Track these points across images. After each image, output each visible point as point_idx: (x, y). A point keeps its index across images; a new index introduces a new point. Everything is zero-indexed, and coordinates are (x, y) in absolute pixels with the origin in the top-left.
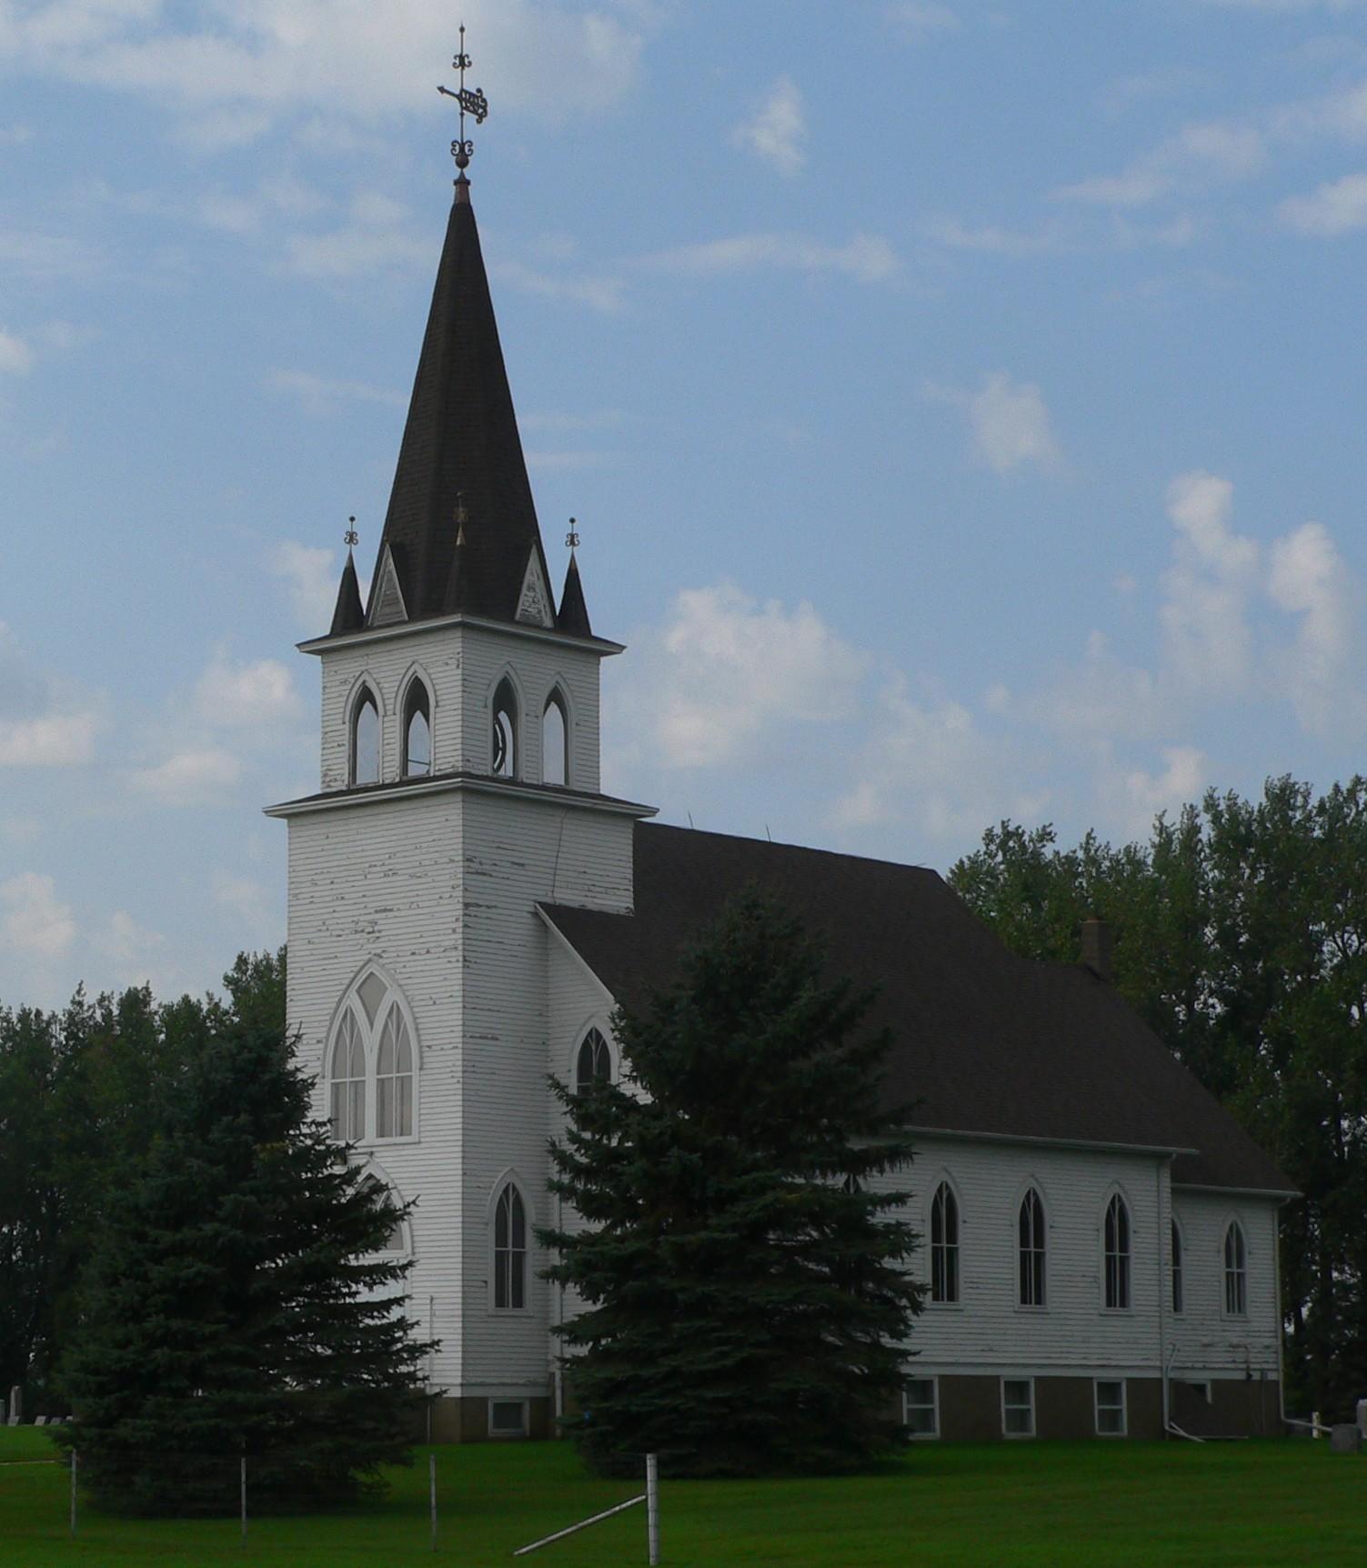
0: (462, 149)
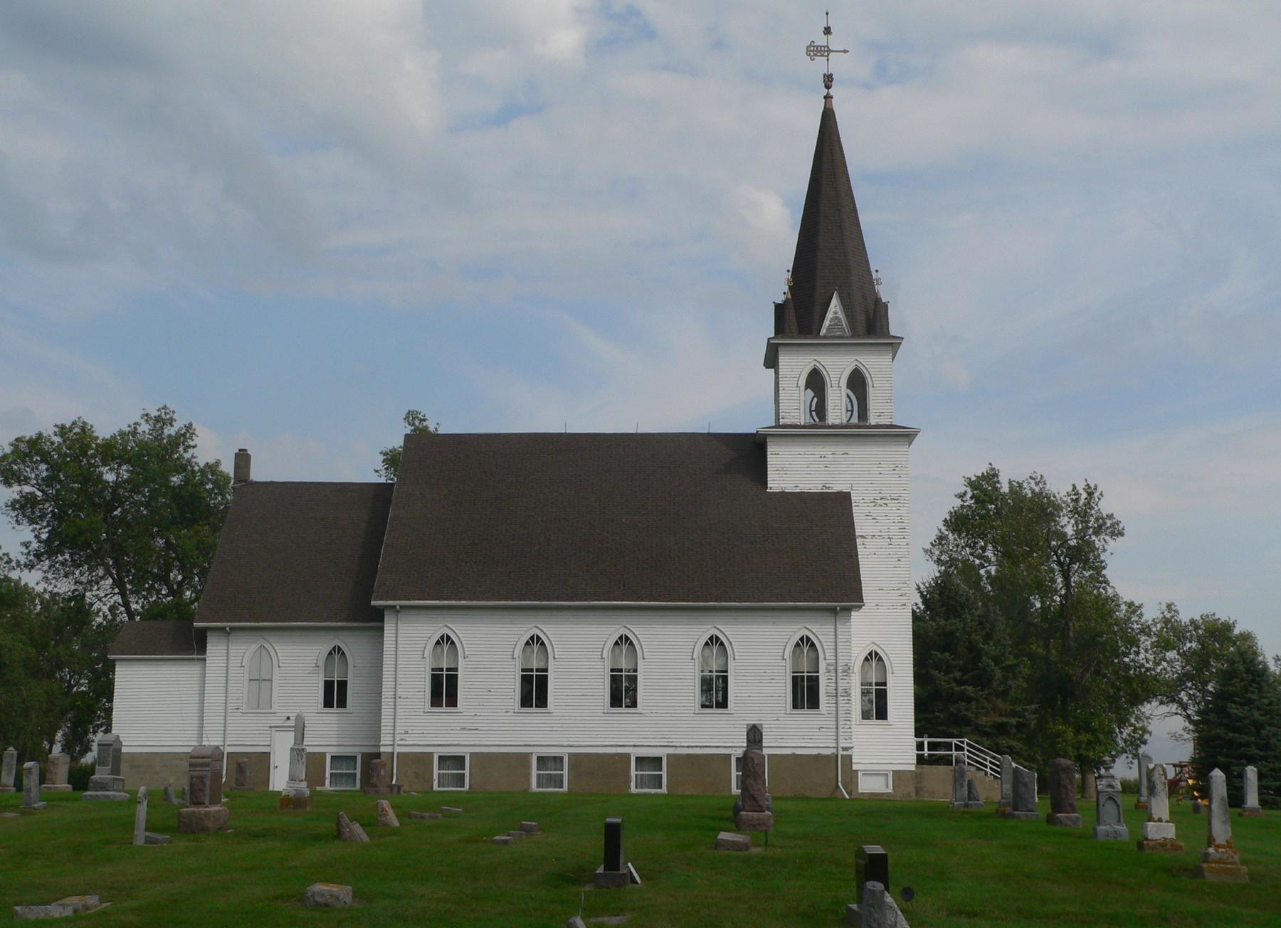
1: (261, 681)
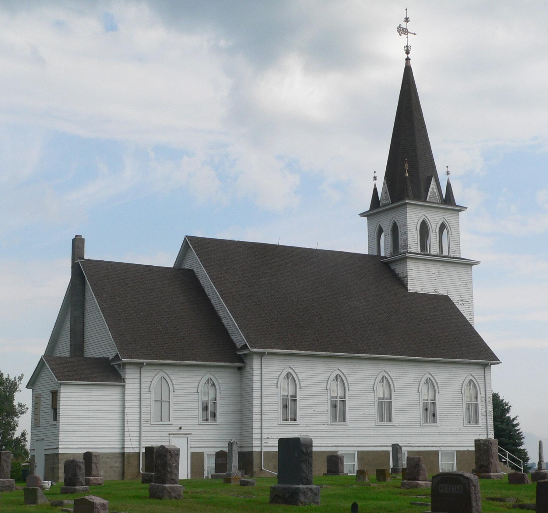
0: (408, 49)
1: (163, 402)
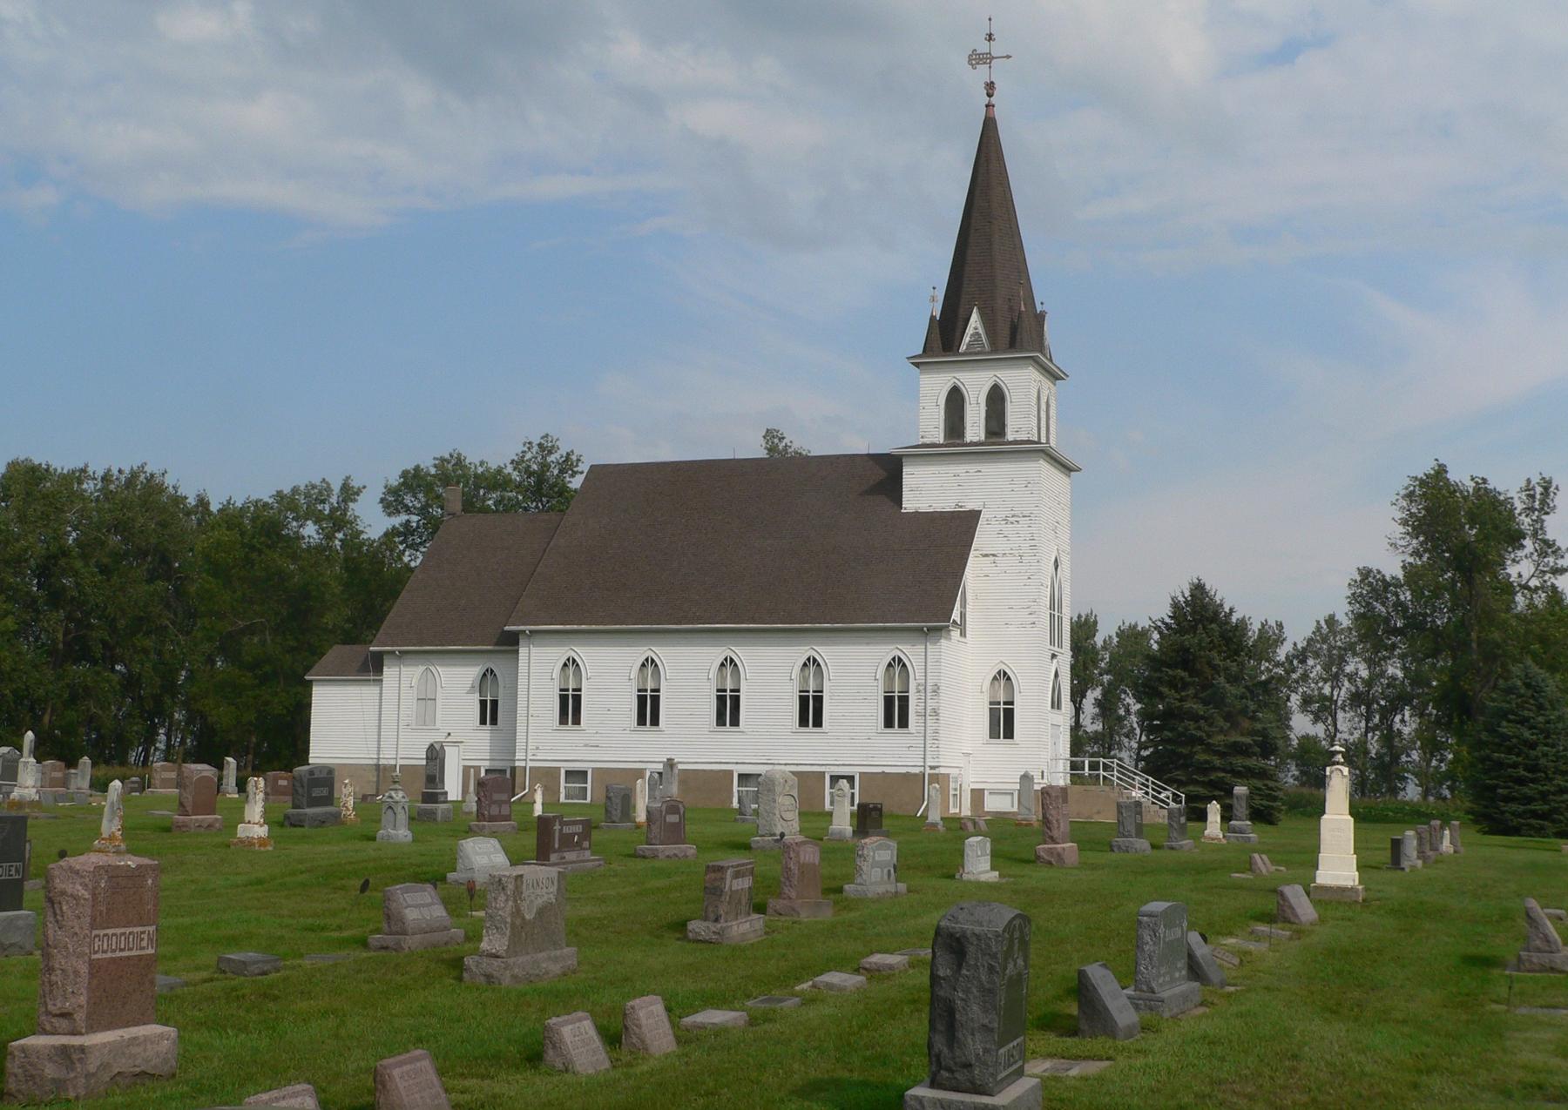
1: (427, 700)
